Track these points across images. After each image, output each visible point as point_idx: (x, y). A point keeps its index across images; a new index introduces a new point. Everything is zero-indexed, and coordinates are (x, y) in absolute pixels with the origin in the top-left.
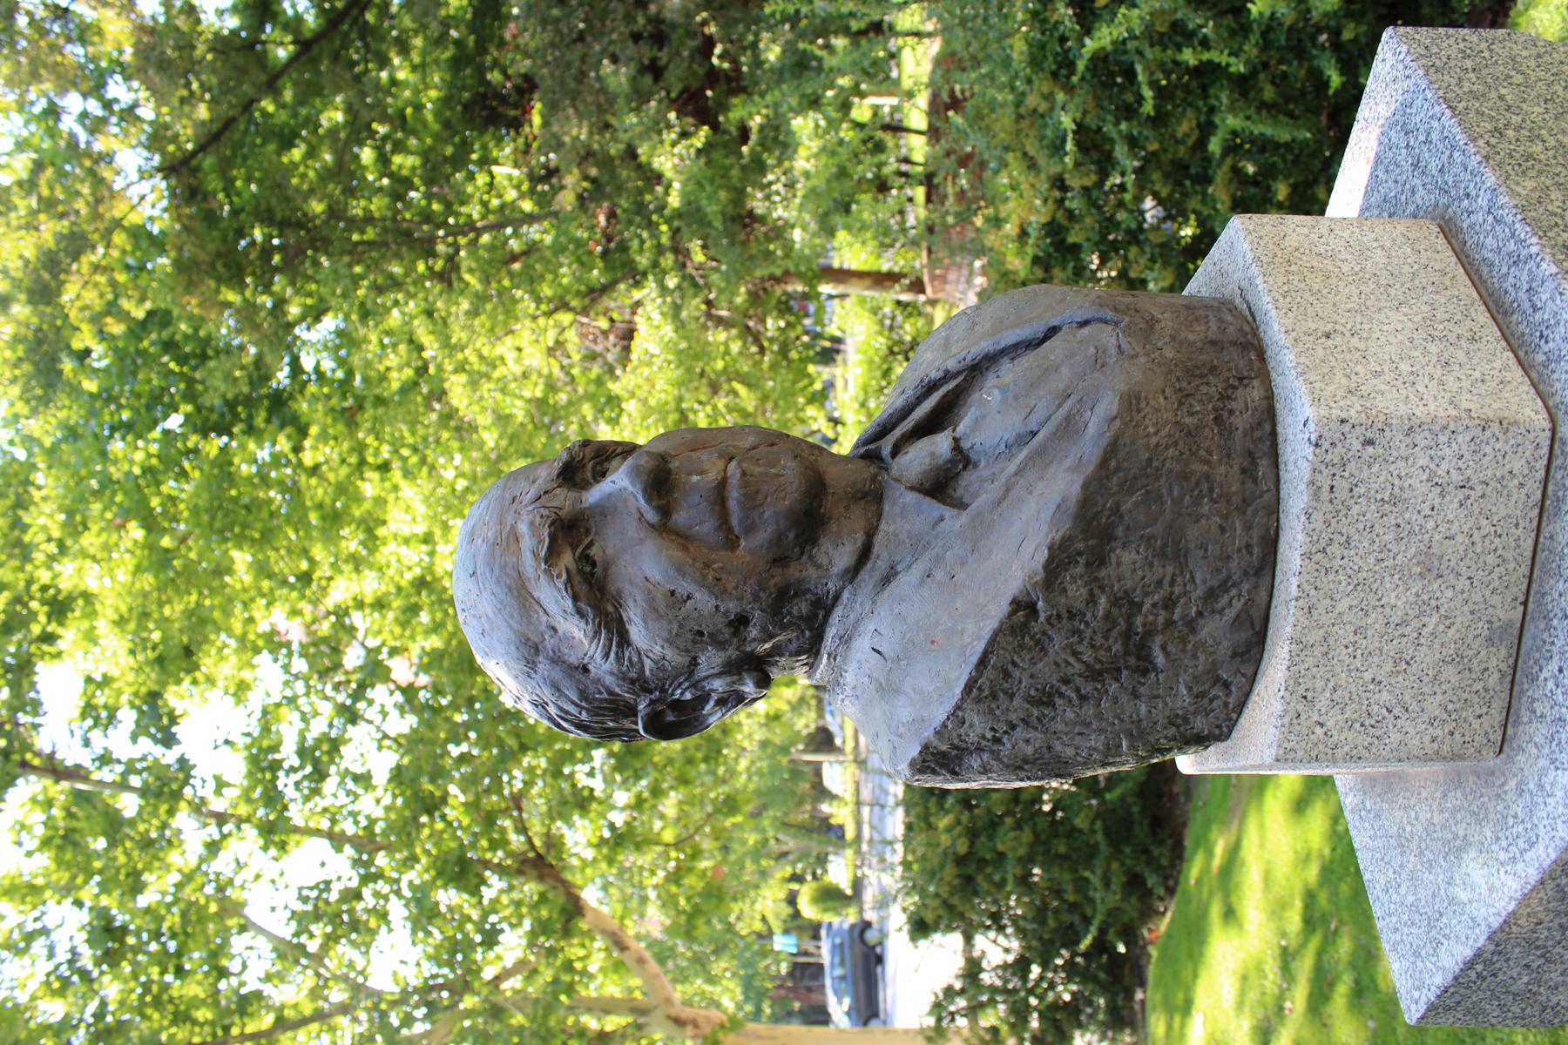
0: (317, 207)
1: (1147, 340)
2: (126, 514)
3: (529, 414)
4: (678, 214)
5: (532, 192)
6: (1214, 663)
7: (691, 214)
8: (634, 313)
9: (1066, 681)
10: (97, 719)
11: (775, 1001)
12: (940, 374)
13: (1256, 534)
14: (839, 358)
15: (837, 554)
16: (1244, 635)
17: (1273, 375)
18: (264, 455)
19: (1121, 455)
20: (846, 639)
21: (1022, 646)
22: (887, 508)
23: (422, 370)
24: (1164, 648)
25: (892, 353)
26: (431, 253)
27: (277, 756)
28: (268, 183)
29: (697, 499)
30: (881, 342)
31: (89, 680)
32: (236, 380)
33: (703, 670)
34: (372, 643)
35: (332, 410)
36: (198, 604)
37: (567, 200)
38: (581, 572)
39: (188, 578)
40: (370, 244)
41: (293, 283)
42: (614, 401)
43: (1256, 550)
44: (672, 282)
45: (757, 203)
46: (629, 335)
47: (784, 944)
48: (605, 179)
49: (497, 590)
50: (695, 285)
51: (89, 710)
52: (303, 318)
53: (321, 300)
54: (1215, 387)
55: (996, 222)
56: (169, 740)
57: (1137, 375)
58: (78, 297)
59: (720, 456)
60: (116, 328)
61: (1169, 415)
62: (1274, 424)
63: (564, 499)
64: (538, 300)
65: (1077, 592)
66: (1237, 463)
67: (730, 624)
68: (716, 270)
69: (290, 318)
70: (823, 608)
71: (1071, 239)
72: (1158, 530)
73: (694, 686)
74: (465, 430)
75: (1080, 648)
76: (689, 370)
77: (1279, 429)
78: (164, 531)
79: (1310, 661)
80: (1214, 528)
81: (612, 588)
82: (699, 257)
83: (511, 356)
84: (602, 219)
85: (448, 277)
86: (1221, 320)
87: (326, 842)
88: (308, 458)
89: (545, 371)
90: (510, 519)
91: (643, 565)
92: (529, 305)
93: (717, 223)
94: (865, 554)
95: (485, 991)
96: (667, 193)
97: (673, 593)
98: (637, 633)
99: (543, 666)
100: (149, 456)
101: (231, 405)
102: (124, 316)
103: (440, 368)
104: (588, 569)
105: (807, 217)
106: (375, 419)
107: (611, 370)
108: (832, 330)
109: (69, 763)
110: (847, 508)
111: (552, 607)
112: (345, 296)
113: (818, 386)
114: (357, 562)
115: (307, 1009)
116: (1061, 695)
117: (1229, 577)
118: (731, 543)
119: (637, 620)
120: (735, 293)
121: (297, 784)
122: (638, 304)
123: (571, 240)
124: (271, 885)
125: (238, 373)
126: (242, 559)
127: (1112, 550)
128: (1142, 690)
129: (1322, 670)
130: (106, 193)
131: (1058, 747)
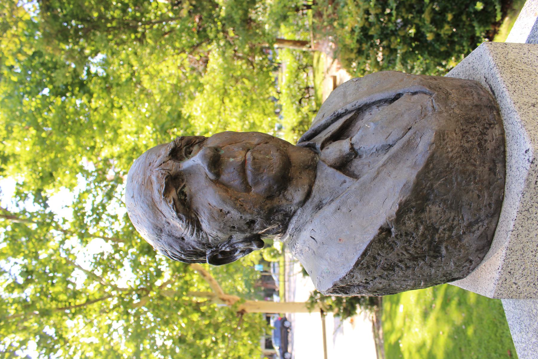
0: (95, 15)
1: (447, 105)
2: (29, 125)
3: (171, 89)
4: (224, 19)
5: (172, 10)
6: (468, 254)
7: (229, 19)
8: (208, 54)
9: (401, 261)
10: (21, 197)
11: (255, 288)
12: (343, 111)
13: (494, 198)
14: (280, 69)
15: (296, 195)
16: (483, 242)
17: (505, 123)
18: (78, 102)
19: (435, 162)
20: (298, 230)
21: (383, 247)
22: (319, 174)
23: (133, 74)
24: (446, 248)
25: (299, 69)
26: (136, 32)
27: (83, 211)
28: (76, 5)
29: (232, 170)
30: (295, 65)
31: (18, 184)
32: (67, 77)
33: (234, 240)
34: (117, 170)
35: (102, 88)
36: (56, 157)
37: (184, 13)
38: (180, 200)
39: (50, 148)
40: (114, 28)
41: (87, 41)
42: (201, 85)
43: (493, 206)
44: (222, 43)
45: (252, 15)
46: (206, 62)
47: (258, 268)
48: (198, 5)
49: (143, 205)
50: (230, 44)
51: (18, 193)
52: (91, 55)
53: (97, 48)
54: (478, 129)
55: (342, 26)
56: (46, 206)
57: (443, 122)
58: (7, 46)
59: (243, 149)
60: (22, 58)
61: (458, 142)
62: (505, 147)
63: (172, 165)
64: (174, 48)
65: (410, 224)
66: (487, 166)
67: (247, 223)
68: (238, 39)
69: (86, 55)
70: (288, 217)
71: (370, 33)
72: (450, 196)
73: (231, 246)
74: (149, 95)
75: (409, 248)
76: (228, 75)
77: (507, 149)
78: (43, 131)
79: (514, 257)
80: (475, 196)
81: (194, 207)
82: (231, 34)
83: (165, 69)
84: (197, 20)
85: (141, 40)
86: (479, 94)
87: (102, 240)
88: (93, 105)
89: (177, 75)
90: (148, 174)
91: (208, 198)
92: (171, 51)
93: (238, 22)
94: (308, 195)
95: (157, 291)
96: (220, 11)
97: (221, 210)
98: (205, 226)
99: (164, 237)
100: (37, 104)
101: (66, 85)
102: (25, 54)
103: (139, 73)
104: (183, 197)
105: (271, 21)
106: (117, 91)
107: (200, 74)
108: (278, 59)
109: (12, 212)
110: (300, 173)
111: (167, 214)
112: (105, 47)
113: (273, 80)
114: (112, 141)
115: (97, 296)
116: (398, 266)
117: (479, 218)
118: (248, 189)
119: (206, 221)
120: (245, 48)
121: (91, 221)
122: (209, 52)
123: (186, 27)
124: (85, 254)
125: (67, 75)
126: (71, 140)
127: (428, 205)
128: (434, 264)
129: (519, 261)
130: (15, 8)
131: (393, 285)
